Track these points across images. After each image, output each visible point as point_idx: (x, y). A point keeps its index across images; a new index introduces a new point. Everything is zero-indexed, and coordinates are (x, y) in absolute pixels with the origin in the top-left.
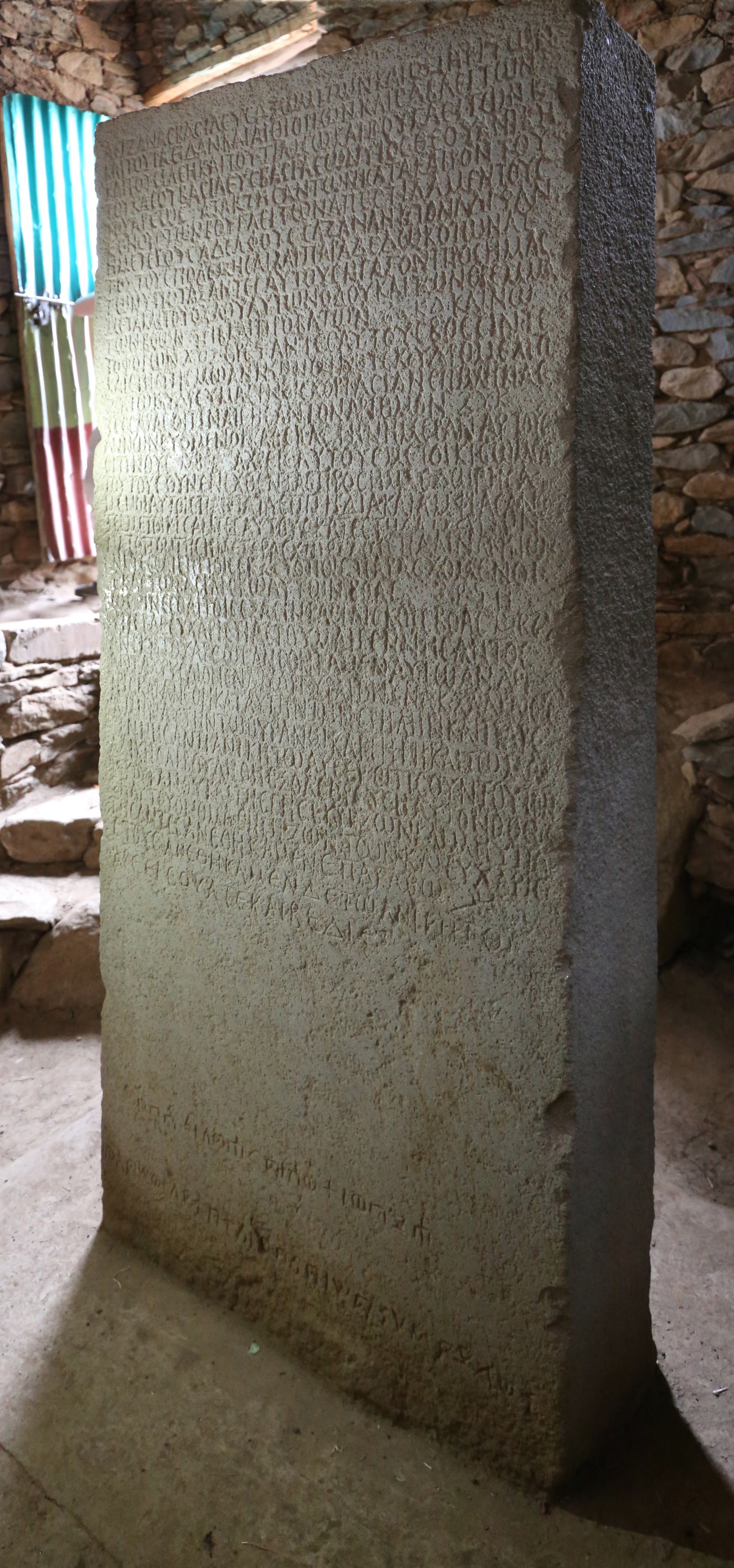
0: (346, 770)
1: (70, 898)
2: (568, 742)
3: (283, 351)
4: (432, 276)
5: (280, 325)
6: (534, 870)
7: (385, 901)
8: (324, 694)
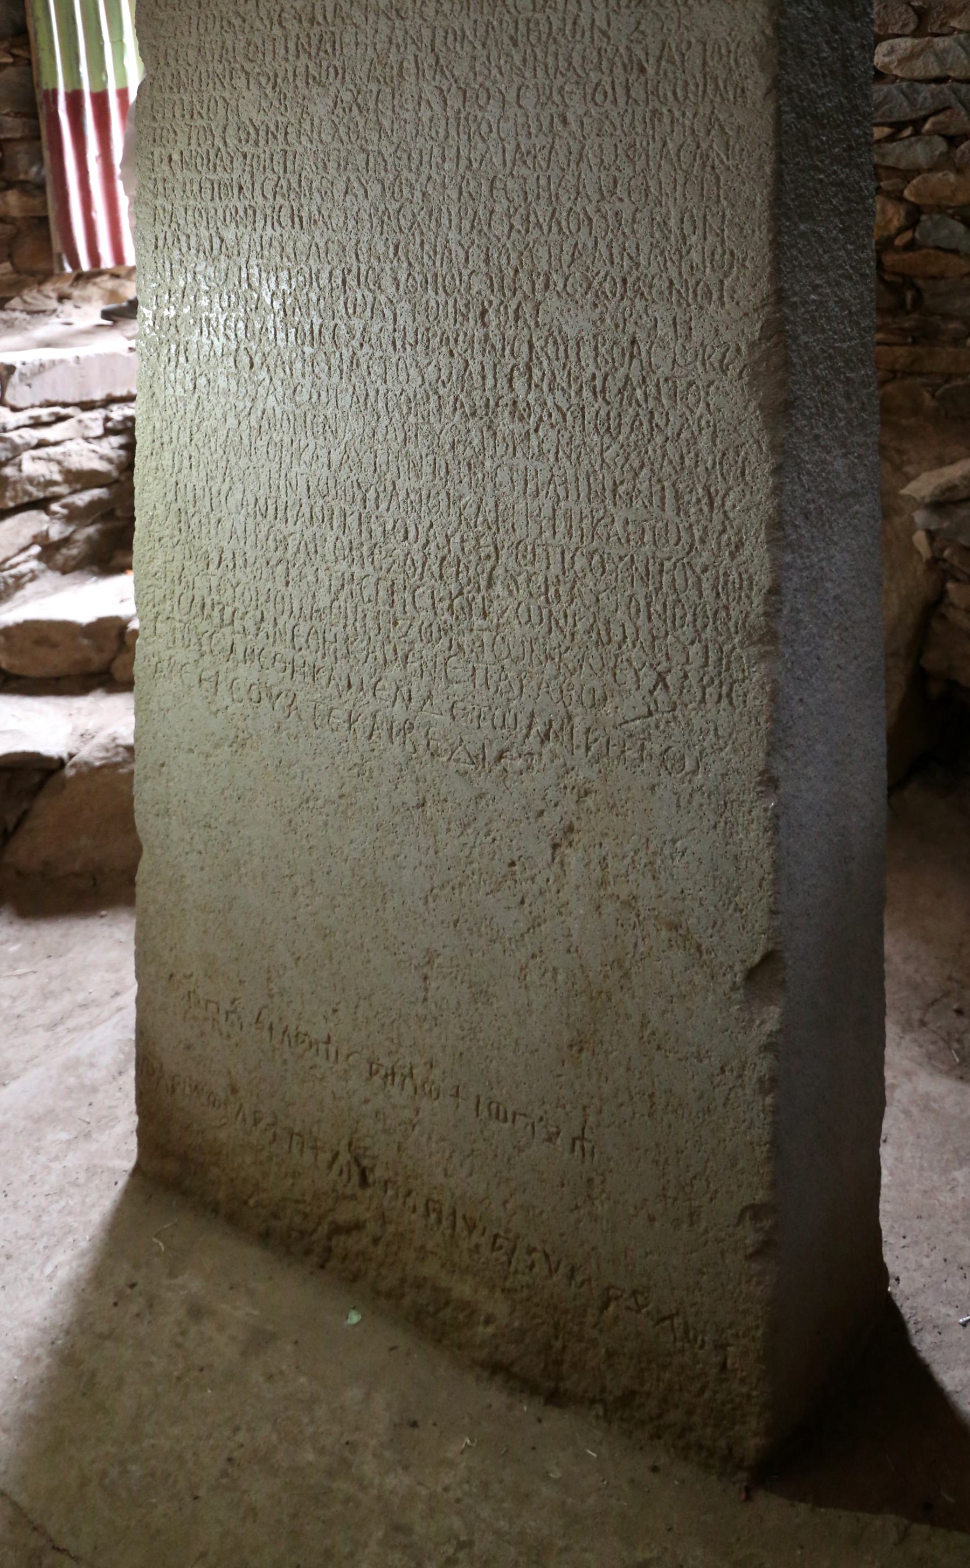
0: (478, 546)
2: (768, 507)
6: (728, 669)
7: (532, 715)
8: (447, 447)
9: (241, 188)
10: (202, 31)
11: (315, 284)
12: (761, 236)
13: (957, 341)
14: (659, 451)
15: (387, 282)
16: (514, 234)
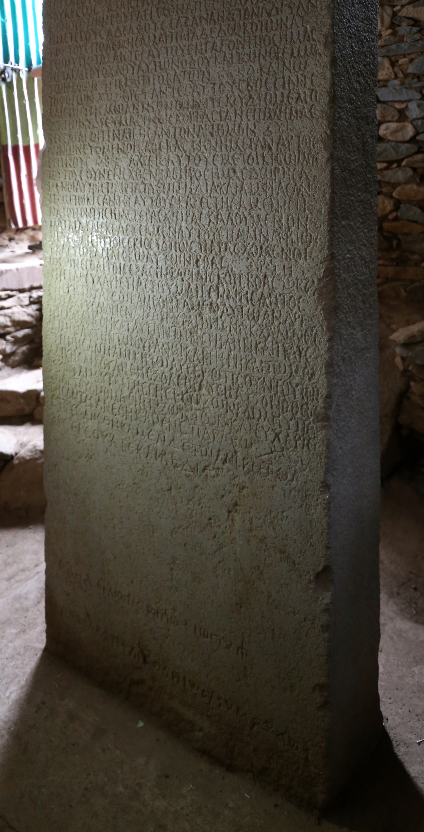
0: (194, 371)
1: (25, 439)
2: (326, 356)
3: (159, 94)
4: (248, 52)
5: (157, 79)
6: (307, 433)
7: (219, 451)
8: (181, 323)
9: (88, 199)
10: (71, 127)
11: (121, 245)
12: (324, 228)
13: (417, 264)
14: (276, 329)
15: (154, 245)
16: (211, 224)
